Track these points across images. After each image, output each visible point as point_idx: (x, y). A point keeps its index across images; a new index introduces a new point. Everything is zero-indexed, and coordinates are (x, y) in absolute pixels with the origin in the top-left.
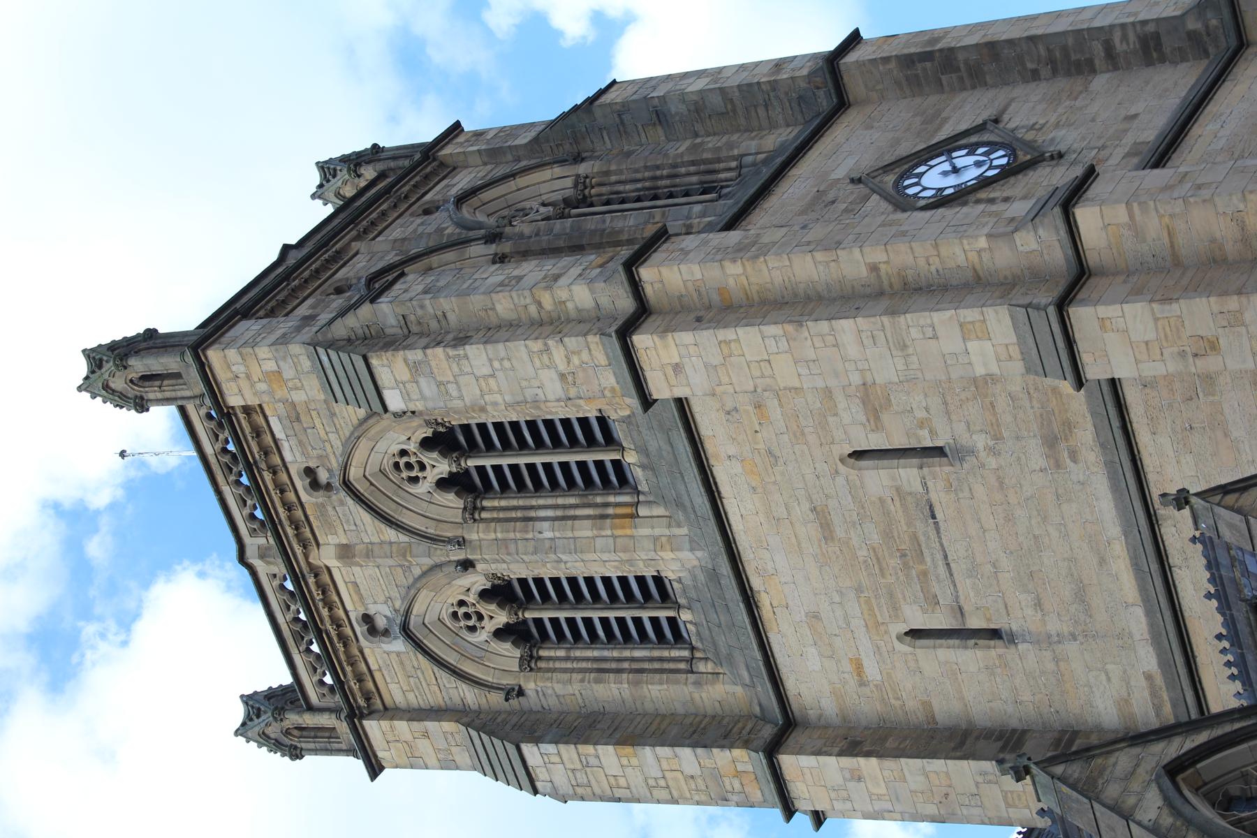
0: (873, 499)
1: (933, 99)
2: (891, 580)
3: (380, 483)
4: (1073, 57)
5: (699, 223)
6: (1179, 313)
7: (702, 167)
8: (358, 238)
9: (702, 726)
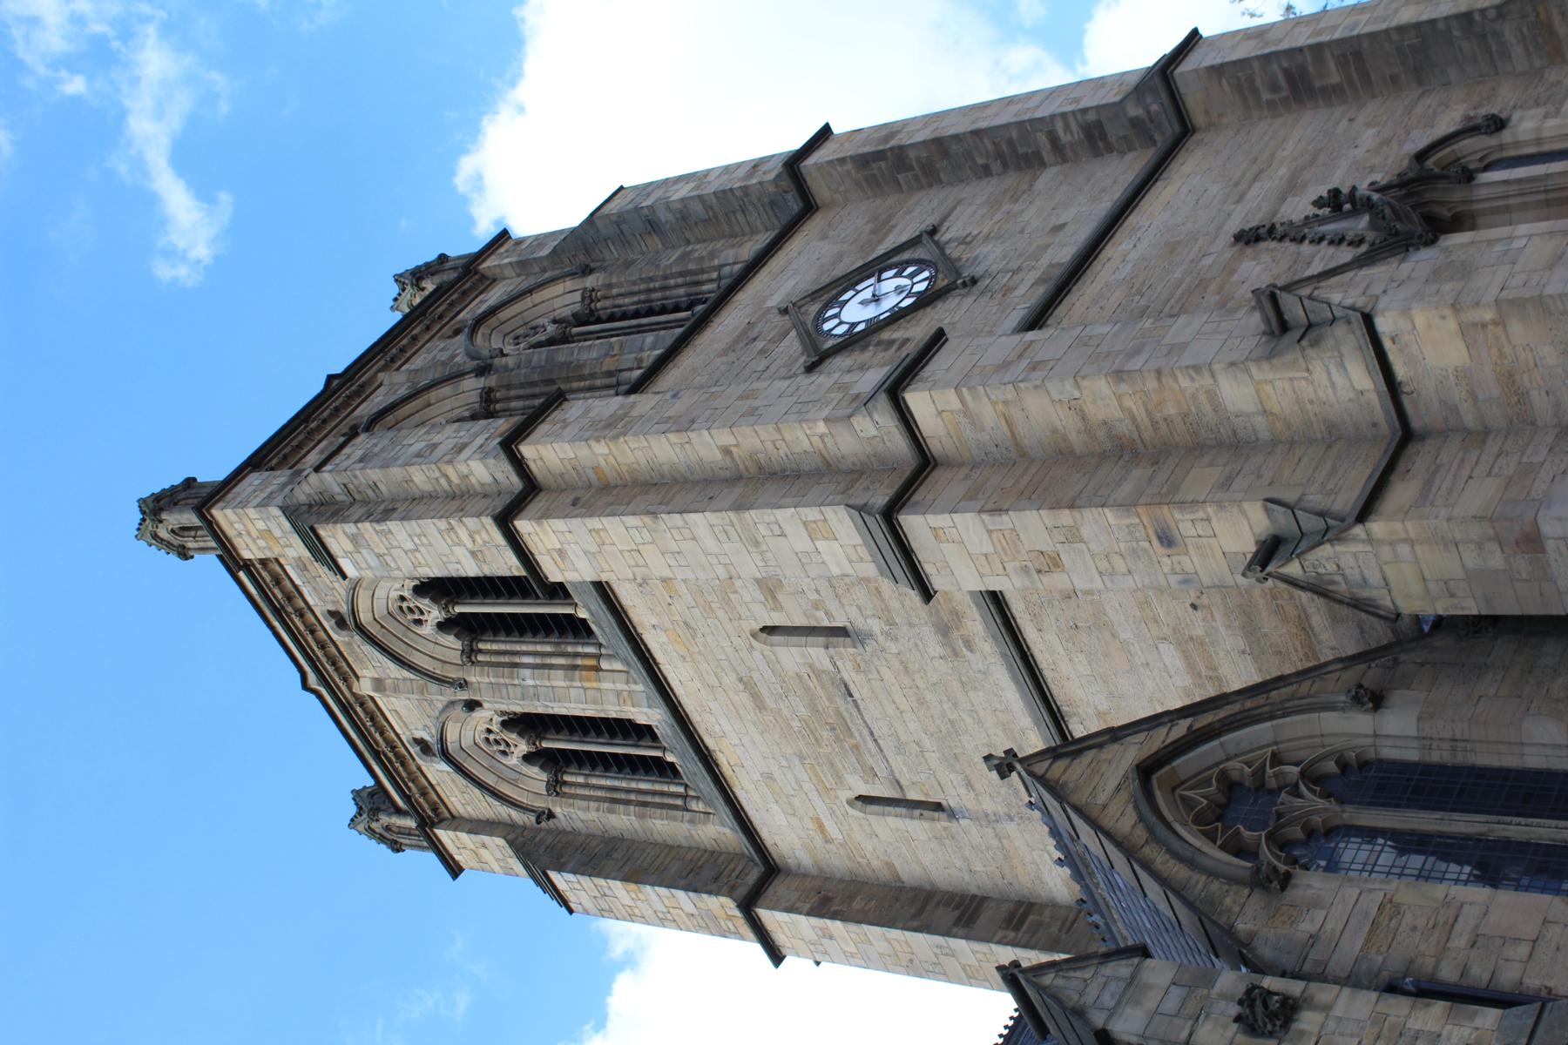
0: (791, 674)
1: (892, 199)
2: (827, 750)
3: (391, 625)
4: (1021, 151)
5: (648, 356)
6: (1011, 526)
7: (688, 279)
8: (384, 368)
9: (700, 864)
